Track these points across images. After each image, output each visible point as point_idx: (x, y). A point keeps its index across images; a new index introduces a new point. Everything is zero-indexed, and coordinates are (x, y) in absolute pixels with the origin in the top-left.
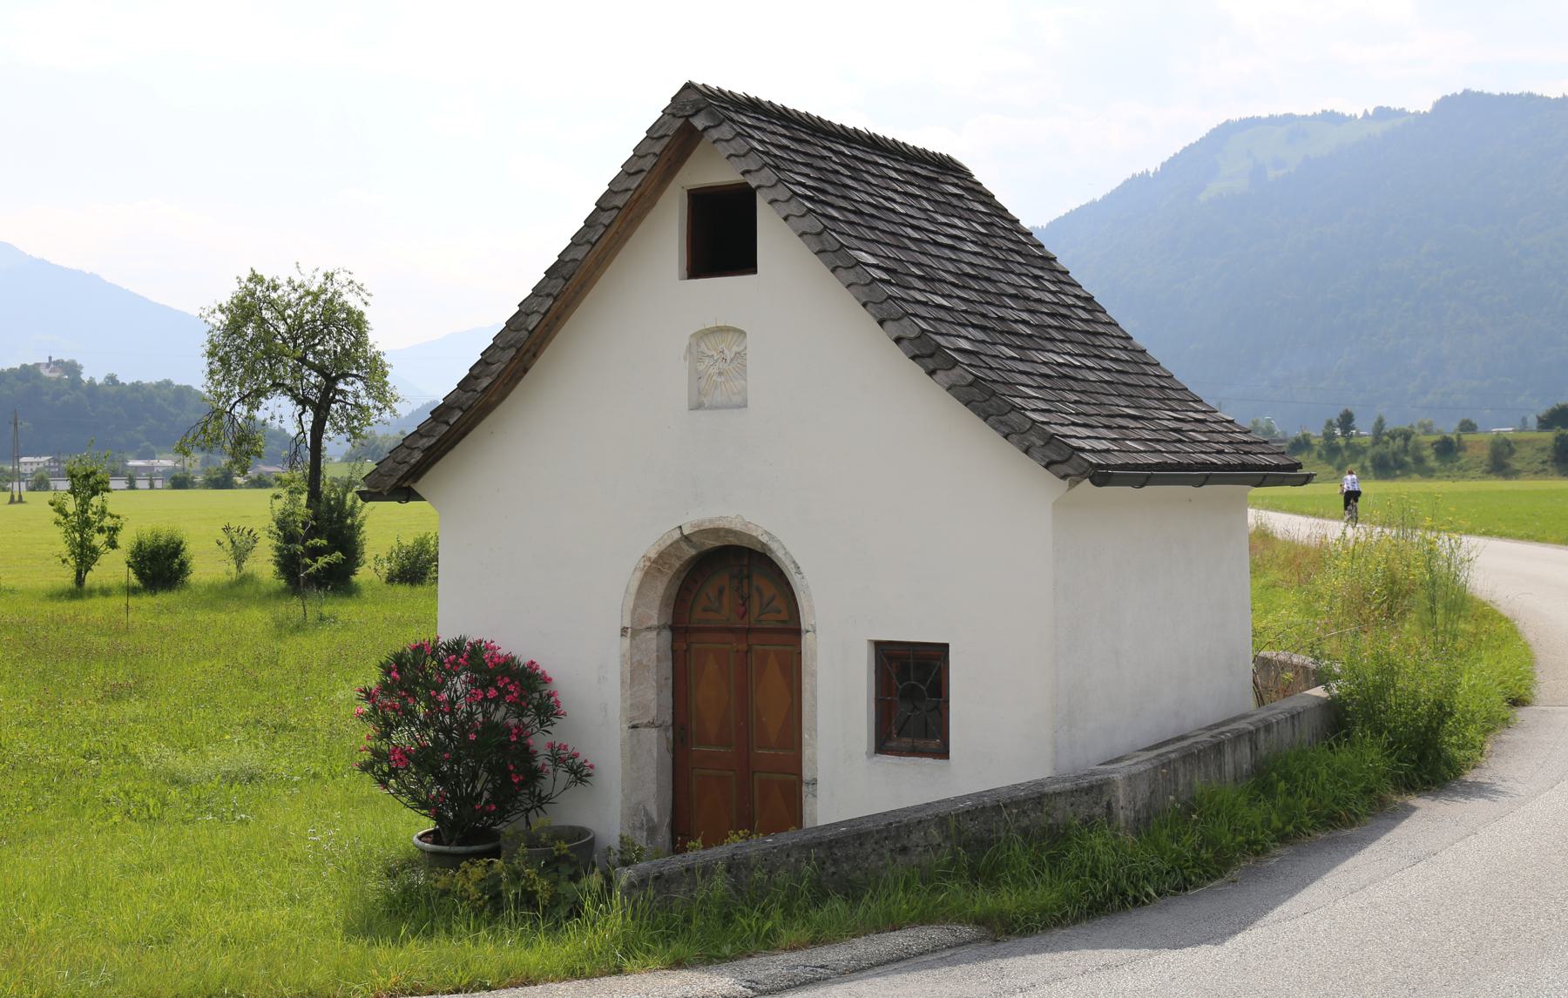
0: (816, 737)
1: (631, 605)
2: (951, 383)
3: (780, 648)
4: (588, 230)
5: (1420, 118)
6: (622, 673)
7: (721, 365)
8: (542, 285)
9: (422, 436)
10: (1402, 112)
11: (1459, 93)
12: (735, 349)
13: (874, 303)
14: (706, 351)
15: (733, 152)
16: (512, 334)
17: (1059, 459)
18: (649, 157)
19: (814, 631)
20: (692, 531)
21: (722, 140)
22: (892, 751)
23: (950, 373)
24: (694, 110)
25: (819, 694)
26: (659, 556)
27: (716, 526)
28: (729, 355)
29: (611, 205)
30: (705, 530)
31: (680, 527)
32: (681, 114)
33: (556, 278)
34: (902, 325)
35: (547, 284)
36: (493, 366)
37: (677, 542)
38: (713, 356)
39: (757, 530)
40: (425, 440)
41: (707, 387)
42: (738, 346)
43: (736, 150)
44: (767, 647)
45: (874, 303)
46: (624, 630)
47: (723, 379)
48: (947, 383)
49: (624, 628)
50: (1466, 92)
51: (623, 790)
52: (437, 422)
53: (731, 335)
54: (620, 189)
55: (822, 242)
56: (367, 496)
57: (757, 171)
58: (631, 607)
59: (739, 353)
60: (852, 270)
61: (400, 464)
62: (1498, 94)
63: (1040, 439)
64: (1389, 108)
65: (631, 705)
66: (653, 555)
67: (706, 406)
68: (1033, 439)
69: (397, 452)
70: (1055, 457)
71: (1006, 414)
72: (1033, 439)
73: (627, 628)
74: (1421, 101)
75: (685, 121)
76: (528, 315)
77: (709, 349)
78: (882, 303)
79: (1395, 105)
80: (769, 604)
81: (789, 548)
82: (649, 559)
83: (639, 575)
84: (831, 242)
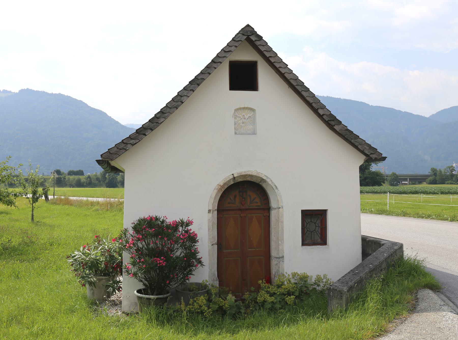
0: (284, 242)
1: (212, 202)
2: (340, 129)
3: (257, 215)
4: (208, 69)
5: (15, 94)
6: (208, 226)
7: (244, 120)
8: (187, 87)
9: (132, 139)
10: (10, 92)
11: (26, 89)
12: (248, 115)
13: (315, 103)
14: (238, 115)
15: (265, 50)
16: (174, 103)
17: (373, 153)
18: (233, 47)
19: (282, 208)
20: (238, 176)
21: (261, 45)
22: (307, 244)
23: (339, 126)
24: (251, 34)
25: (284, 228)
26: (224, 184)
27: (247, 174)
28: (246, 117)
29: (218, 61)
30: (243, 175)
31: (233, 174)
32: (246, 34)
33: (194, 84)
34: (324, 110)
35: (190, 86)
36: (165, 114)
37: (231, 179)
38: (240, 117)
39: (262, 175)
40: (133, 141)
41: (238, 127)
42: (250, 114)
43: (267, 49)
44: (252, 215)
45: (315, 103)
46: (209, 211)
47: (244, 125)
48: (339, 129)
49: (209, 210)
50: (27, 89)
51: (209, 267)
52: (139, 134)
53: (247, 111)
54: (222, 56)
55: (297, 82)
56: (101, 162)
57: (274, 57)
58: (213, 203)
59: (250, 117)
60: (307, 92)
61: (121, 149)
62: (36, 90)
63: (367, 147)
64: (7, 90)
65: (212, 237)
66: (222, 184)
67: (237, 134)
68: (366, 147)
69: (119, 145)
70: (372, 152)
71: (357, 139)
72: (366, 147)
73: (211, 210)
74: (16, 90)
75: (247, 37)
76: (181, 96)
77: (239, 115)
78: (317, 103)
79: (9, 89)
80: (253, 201)
81: (273, 181)
82: (220, 186)
83: (216, 191)
84: (300, 82)
